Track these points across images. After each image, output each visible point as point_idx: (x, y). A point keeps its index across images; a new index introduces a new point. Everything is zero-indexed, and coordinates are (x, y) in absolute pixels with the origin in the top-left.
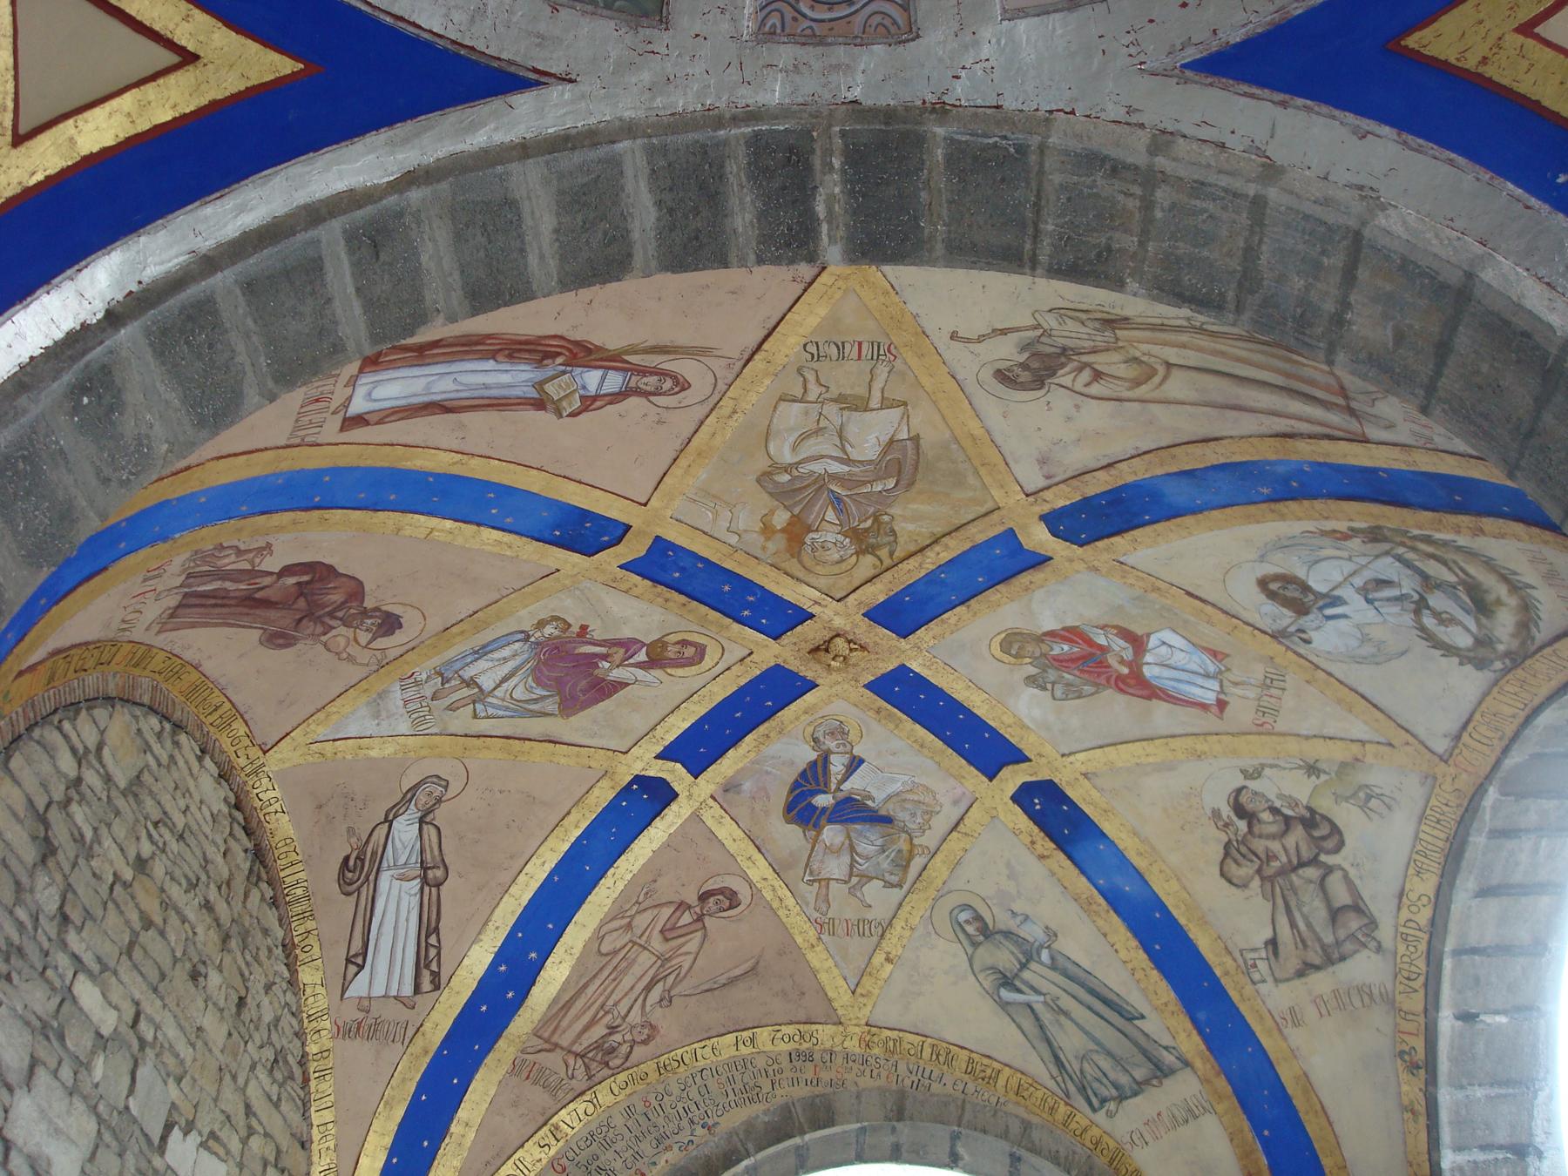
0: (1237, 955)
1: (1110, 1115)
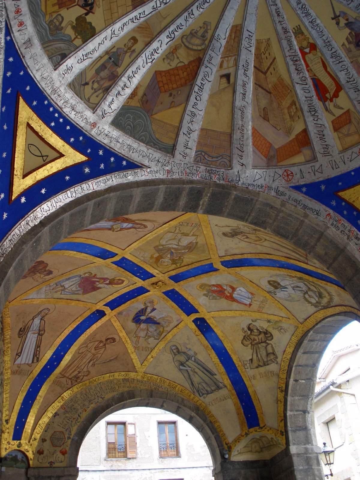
0: (242, 362)
1: (204, 398)
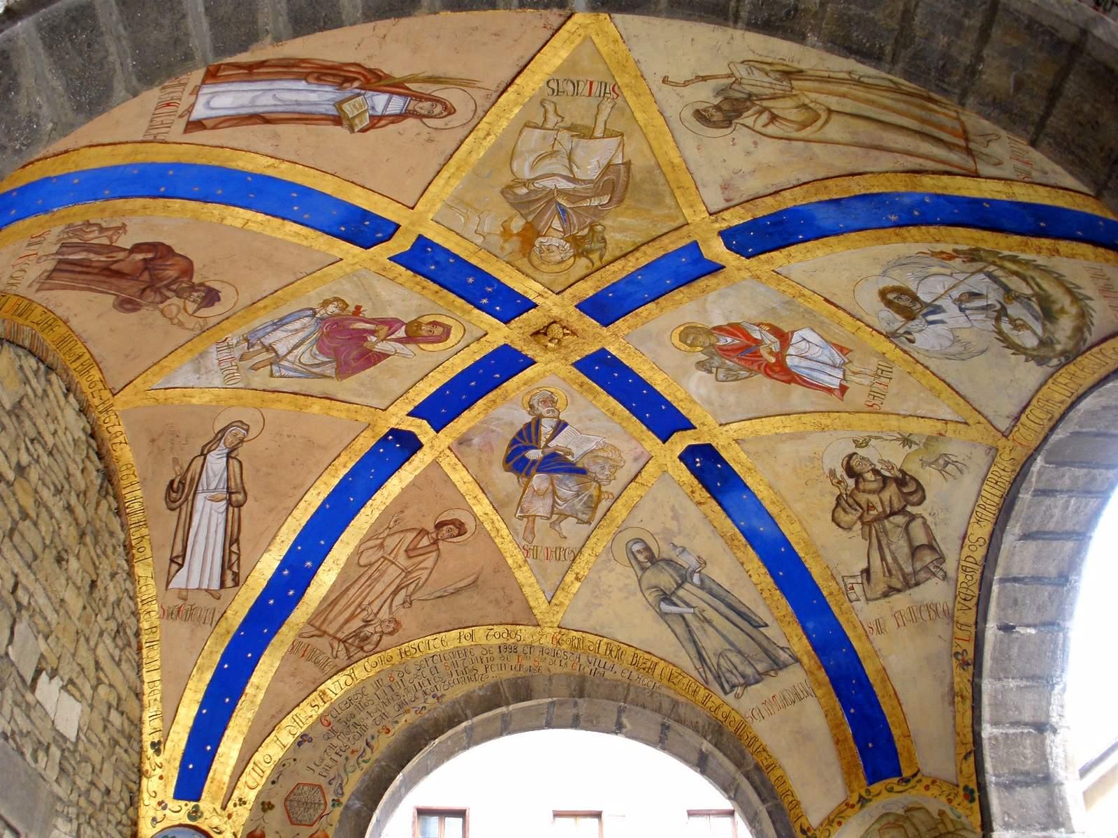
0: (840, 580)
1: (737, 697)
